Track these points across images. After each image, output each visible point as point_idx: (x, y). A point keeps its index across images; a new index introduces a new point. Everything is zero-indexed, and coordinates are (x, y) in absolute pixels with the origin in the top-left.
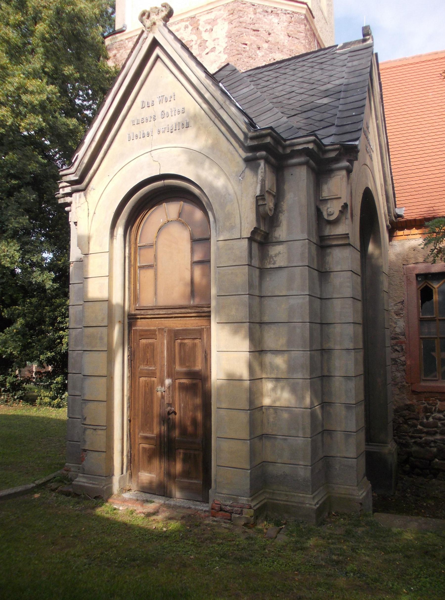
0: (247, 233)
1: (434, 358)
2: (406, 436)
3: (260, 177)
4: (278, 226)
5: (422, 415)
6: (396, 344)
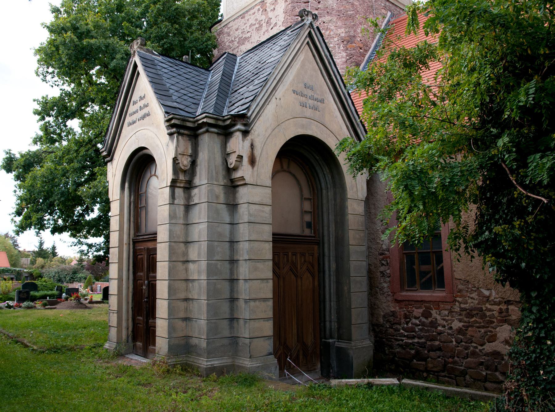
0: (169, 184)
1: (414, 269)
2: (392, 339)
3: (175, 146)
4: (196, 176)
5: (403, 321)
6: (383, 259)
